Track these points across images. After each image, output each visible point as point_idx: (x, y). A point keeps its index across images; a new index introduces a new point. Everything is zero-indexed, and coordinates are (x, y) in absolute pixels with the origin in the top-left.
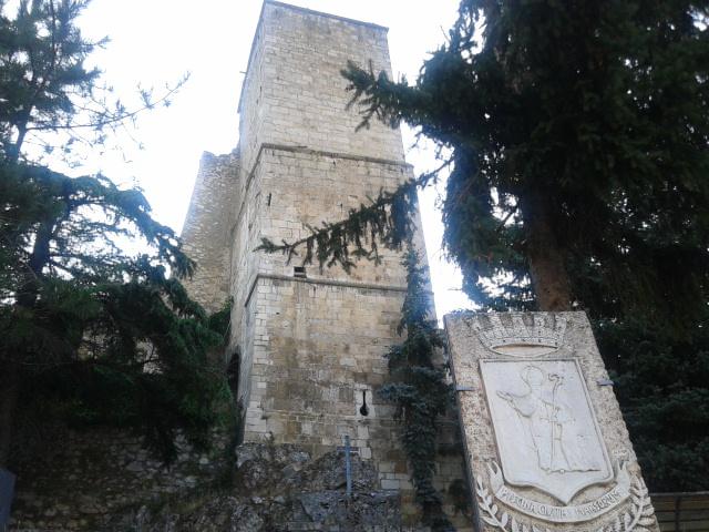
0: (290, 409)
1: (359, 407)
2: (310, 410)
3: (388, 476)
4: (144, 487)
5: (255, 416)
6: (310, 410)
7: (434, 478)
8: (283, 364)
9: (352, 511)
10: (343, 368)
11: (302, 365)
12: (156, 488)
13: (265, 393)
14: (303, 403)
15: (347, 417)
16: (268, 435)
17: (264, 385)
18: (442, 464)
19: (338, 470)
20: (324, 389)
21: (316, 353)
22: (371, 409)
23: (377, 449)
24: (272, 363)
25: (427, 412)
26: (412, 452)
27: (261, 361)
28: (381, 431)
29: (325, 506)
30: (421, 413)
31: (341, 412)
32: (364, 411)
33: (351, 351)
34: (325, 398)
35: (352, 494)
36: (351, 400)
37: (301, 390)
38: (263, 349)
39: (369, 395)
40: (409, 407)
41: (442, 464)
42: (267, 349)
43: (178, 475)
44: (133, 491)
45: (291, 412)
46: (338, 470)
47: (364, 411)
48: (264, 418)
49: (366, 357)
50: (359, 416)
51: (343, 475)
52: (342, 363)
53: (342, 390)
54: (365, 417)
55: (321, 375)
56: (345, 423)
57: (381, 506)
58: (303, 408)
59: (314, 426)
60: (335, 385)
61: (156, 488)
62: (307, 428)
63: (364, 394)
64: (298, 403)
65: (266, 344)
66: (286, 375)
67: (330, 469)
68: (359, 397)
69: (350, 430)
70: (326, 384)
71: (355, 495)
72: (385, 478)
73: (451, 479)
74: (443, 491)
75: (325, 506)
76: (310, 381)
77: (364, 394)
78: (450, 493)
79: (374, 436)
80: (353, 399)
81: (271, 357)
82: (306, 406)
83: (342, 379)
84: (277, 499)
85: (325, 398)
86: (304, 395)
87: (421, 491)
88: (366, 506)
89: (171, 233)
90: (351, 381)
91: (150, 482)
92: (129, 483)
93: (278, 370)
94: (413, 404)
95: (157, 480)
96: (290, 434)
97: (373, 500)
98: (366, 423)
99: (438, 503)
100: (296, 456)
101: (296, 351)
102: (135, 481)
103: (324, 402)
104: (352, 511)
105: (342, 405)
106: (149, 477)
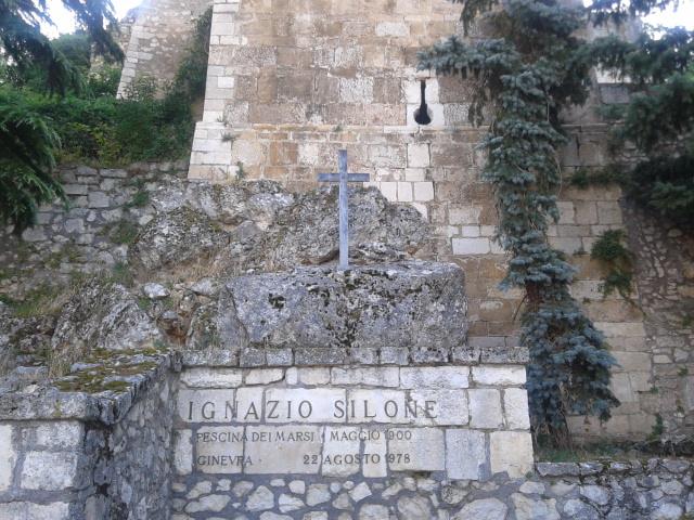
0: (279, 121)
1: (412, 110)
2: (317, 121)
3: (467, 231)
4: (47, 266)
5: (210, 136)
6: (317, 121)
7: (552, 232)
8: (268, 41)
9: (341, 311)
10: (383, 43)
11: (303, 41)
12: (66, 267)
13: (230, 96)
14: (304, 109)
15: (387, 130)
16: (233, 171)
17: (230, 82)
18: (578, 204)
19: (326, 224)
20: (344, 82)
21: (329, 17)
22: (437, 112)
23: (446, 183)
24: (245, 41)
25: (536, 92)
26: (502, 177)
27: (224, 41)
28: (457, 150)
29: (277, 302)
30: (522, 95)
31: (376, 119)
32: (423, 116)
33: (398, 10)
34: (346, 97)
35: (347, 273)
36: (396, 96)
37: (300, 87)
38: (230, 17)
39: (433, 88)
40: (497, 85)
41: (578, 204)
42: (237, 17)
43: (103, 245)
44: (30, 274)
45: (278, 127)
46: (326, 224)
47: (423, 116)
48: (226, 139)
49: (428, 19)
50: (412, 125)
51: (334, 233)
52: (380, 32)
53: (378, 83)
54: (423, 127)
55: (340, 57)
56: (384, 140)
57: (409, 299)
58: (303, 119)
59: (323, 148)
60: (367, 72)
61: (66, 267)
62: (309, 153)
63: (423, 87)
64: (293, 109)
65: (236, 8)
66: (272, 61)
67: (310, 221)
68: (412, 94)
69: (392, 152)
70: (349, 72)
71: (353, 276)
72: (460, 235)
73: (598, 231)
74: (581, 253)
75: (277, 302)
76: (318, 70)
77: (423, 87)
78: (594, 255)
79: (440, 161)
80: (402, 95)
81: (244, 31)
82: (308, 115)
83: (379, 62)
84: (199, 287)
85: (346, 97)
86: (307, 94)
87: (519, 260)
88: (374, 299)
89: (472, 107)
90: (397, 63)
91: (58, 257)
92: (24, 260)
93: (258, 53)
94: (505, 77)
95: (66, 252)
96: (276, 165)
97: (390, 287)
98: (425, 138)
99: (559, 283)
100: (264, 202)
101: (290, 16)
102: (34, 257)
103: (344, 105)
104: (341, 311)
105: (380, 109)
106: (56, 249)
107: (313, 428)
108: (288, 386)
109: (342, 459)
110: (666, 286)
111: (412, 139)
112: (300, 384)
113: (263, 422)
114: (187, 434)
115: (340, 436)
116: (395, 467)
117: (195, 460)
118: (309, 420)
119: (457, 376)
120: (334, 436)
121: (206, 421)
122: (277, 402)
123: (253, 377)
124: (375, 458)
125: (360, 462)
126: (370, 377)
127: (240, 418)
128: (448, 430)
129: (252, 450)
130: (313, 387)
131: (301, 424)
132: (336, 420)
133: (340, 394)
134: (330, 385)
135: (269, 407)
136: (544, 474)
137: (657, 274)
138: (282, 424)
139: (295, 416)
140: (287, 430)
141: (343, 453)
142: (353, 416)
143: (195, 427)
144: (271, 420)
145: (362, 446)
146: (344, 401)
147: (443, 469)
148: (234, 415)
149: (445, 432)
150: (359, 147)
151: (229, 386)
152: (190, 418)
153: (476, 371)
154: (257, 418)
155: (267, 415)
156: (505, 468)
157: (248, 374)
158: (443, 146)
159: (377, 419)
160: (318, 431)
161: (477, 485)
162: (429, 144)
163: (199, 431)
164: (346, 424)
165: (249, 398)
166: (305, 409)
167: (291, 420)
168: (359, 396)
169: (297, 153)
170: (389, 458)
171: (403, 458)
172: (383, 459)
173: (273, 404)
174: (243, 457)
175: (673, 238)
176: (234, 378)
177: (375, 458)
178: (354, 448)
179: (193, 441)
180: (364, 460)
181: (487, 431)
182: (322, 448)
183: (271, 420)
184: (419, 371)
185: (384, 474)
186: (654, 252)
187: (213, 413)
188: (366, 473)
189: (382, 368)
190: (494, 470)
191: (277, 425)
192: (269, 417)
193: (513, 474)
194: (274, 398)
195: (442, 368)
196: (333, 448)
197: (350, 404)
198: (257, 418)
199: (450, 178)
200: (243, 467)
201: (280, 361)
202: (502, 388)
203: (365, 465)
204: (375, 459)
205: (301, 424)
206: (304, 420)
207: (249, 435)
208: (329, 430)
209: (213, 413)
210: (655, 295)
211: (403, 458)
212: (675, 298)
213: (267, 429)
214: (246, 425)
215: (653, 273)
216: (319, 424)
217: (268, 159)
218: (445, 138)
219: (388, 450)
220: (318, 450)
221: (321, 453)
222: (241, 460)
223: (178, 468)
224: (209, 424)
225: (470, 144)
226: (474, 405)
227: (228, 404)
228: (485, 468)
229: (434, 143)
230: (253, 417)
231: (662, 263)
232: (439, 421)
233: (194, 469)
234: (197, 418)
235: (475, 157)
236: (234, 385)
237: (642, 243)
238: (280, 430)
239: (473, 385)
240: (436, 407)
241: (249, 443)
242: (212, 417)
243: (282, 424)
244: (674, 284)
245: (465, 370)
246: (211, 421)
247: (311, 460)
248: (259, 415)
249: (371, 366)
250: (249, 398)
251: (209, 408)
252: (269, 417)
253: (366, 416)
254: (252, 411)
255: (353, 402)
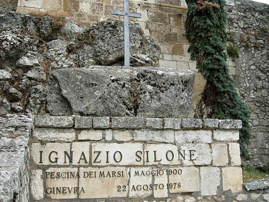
28: (160, 16)
79: (154, 20)
107: (123, 169)
108: (106, 142)
109: (142, 187)
110: (249, 91)
111: (139, 6)
112: (114, 141)
113: (91, 165)
114: (39, 172)
115: (140, 173)
116: (172, 191)
117: (46, 191)
118: (121, 163)
119: (205, 136)
120: (137, 173)
121: (52, 164)
122: (100, 152)
123: (83, 135)
124: (161, 187)
125: (152, 189)
126: (157, 136)
127: (75, 162)
128: (201, 168)
129: (83, 183)
130: (122, 142)
131: (115, 166)
132: (137, 163)
133: (139, 147)
134: (133, 141)
135: (94, 156)
136: (248, 189)
137: (247, 85)
138: (103, 167)
139: (112, 161)
140: (106, 170)
141: (142, 184)
142: (148, 161)
143: (44, 168)
144: (95, 164)
145: (153, 179)
146: (142, 151)
147: (199, 191)
148: (71, 161)
149: (200, 169)
150: (112, 7)
151: (66, 140)
152: (41, 162)
153: (216, 133)
154: (86, 162)
155: (93, 160)
156: (230, 187)
157: (80, 133)
158: (155, 12)
159: (162, 163)
160: (126, 170)
161: (216, 198)
162: (147, 10)
163: (47, 171)
164: (143, 166)
165: (80, 149)
166: (118, 157)
167: (109, 164)
168: (151, 148)
169: (78, 6)
170: (169, 186)
171: (177, 185)
172: (166, 187)
173: (97, 154)
174: (78, 188)
175: (252, 70)
176: (71, 135)
177: (161, 187)
178: (149, 182)
179: (44, 177)
180: (155, 188)
181: (220, 167)
182: (129, 181)
183: (95, 164)
184: (185, 133)
185: (166, 195)
186: (245, 75)
187: (57, 159)
188: (155, 196)
189: (164, 131)
190: (225, 189)
191: (99, 167)
192: (95, 162)
193: (233, 191)
194: (97, 149)
195: (198, 132)
196: (135, 181)
197: (146, 153)
198: (86, 162)
199: (158, 29)
200: (78, 195)
201: (102, 125)
202: (227, 143)
203: (155, 191)
204: (161, 187)
205: (115, 166)
206: (117, 164)
207: (81, 174)
208: (133, 170)
209: (57, 159)
210: (246, 95)
211: (177, 185)
212: (253, 97)
213: (94, 170)
214: (79, 167)
215: (245, 85)
216: (127, 166)
217: (62, 8)
218: (156, 9)
219: (168, 181)
220: (127, 182)
221: (128, 184)
222: (77, 190)
223: (34, 196)
224: (54, 166)
225: (167, 13)
226: (215, 153)
227: (66, 153)
228: (220, 188)
229: (150, 10)
230: (83, 161)
231: (248, 80)
232: (197, 163)
233: (45, 197)
234: (46, 162)
235: (170, 20)
236: (71, 141)
237: (241, 71)
238: (102, 170)
239: (215, 141)
240: (195, 153)
241: (82, 178)
242: (56, 162)
243: (103, 167)
244: (253, 90)
245: (210, 132)
246: (55, 164)
247: (122, 189)
248: (88, 160)
249: (157, 130)
250: (80, 149)
251: (53, 156)
252: (95, 162)
253: (155, 161)
254: (82, 157)
255: (147, 152)
